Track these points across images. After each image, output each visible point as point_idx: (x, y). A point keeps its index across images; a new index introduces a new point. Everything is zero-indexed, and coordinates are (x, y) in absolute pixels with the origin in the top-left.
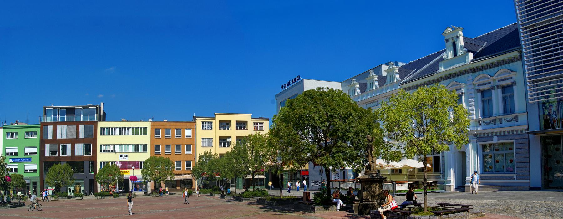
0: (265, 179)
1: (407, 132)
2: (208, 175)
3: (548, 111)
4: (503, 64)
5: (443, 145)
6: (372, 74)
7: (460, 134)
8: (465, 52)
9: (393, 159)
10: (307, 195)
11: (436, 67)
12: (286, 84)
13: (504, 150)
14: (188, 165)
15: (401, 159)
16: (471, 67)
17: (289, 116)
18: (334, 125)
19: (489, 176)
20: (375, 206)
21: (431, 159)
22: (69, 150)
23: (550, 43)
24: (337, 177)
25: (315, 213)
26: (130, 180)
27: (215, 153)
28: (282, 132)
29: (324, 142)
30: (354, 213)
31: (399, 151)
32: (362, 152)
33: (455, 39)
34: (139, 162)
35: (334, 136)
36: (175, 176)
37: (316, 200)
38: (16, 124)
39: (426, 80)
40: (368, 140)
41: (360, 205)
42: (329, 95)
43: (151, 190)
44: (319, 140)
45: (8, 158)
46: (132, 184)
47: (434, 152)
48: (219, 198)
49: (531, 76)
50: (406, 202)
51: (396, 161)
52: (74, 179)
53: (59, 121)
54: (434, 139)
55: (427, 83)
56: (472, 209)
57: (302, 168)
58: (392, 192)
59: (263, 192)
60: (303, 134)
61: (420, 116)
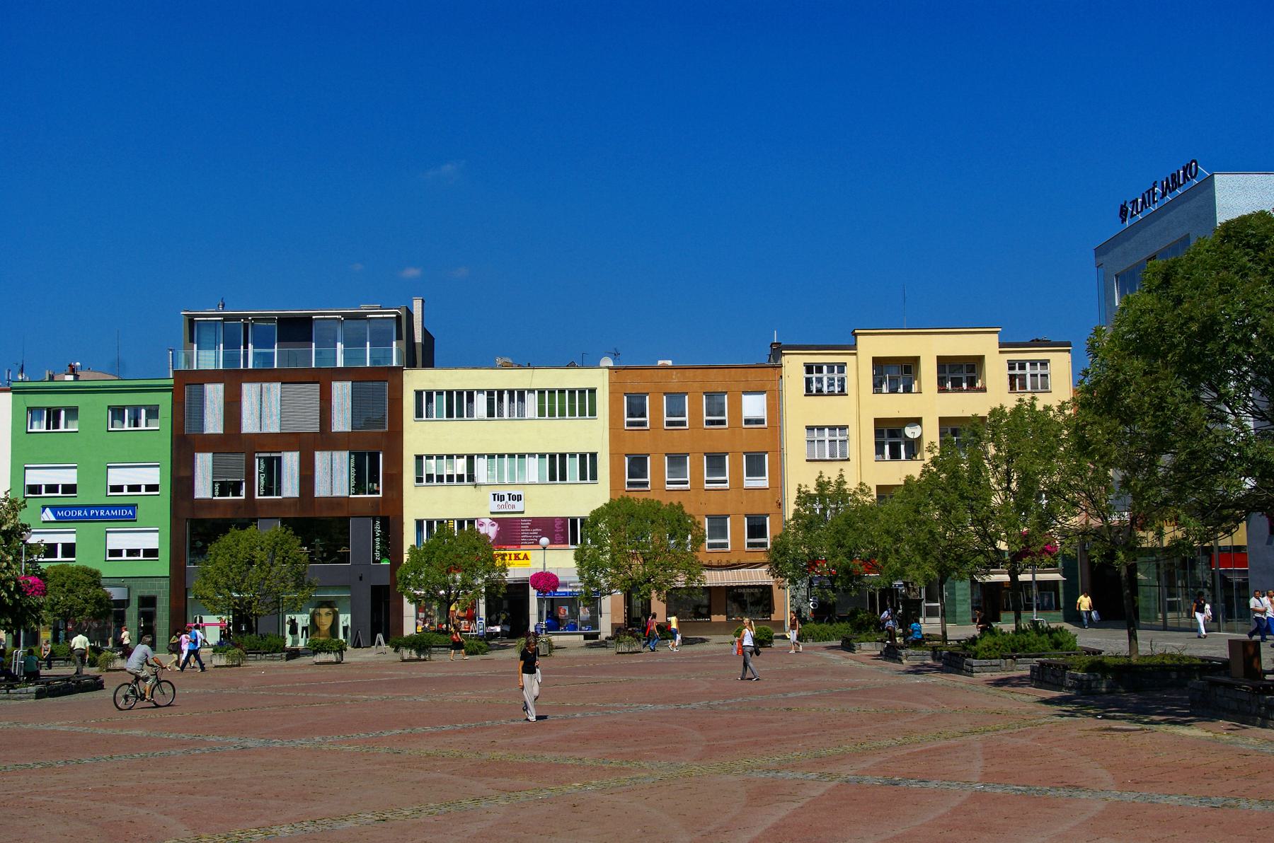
0: (1061, 585)
2: (834, 567)
12: (1140, 200)
14: (757, 529)
17: (1160, 329)
22: (292, 477)
26: (531, 588)
27: (861, 484)
28: (1132, 394)
34: (564, 519)
36: (706, 573)
38: (71, 378)
43: (612, 624)
45: (34, 503)
46: (540, 602)
48: (876, 658)
52: (310, 585)
53: (250, 366)
59: (1056, 635)
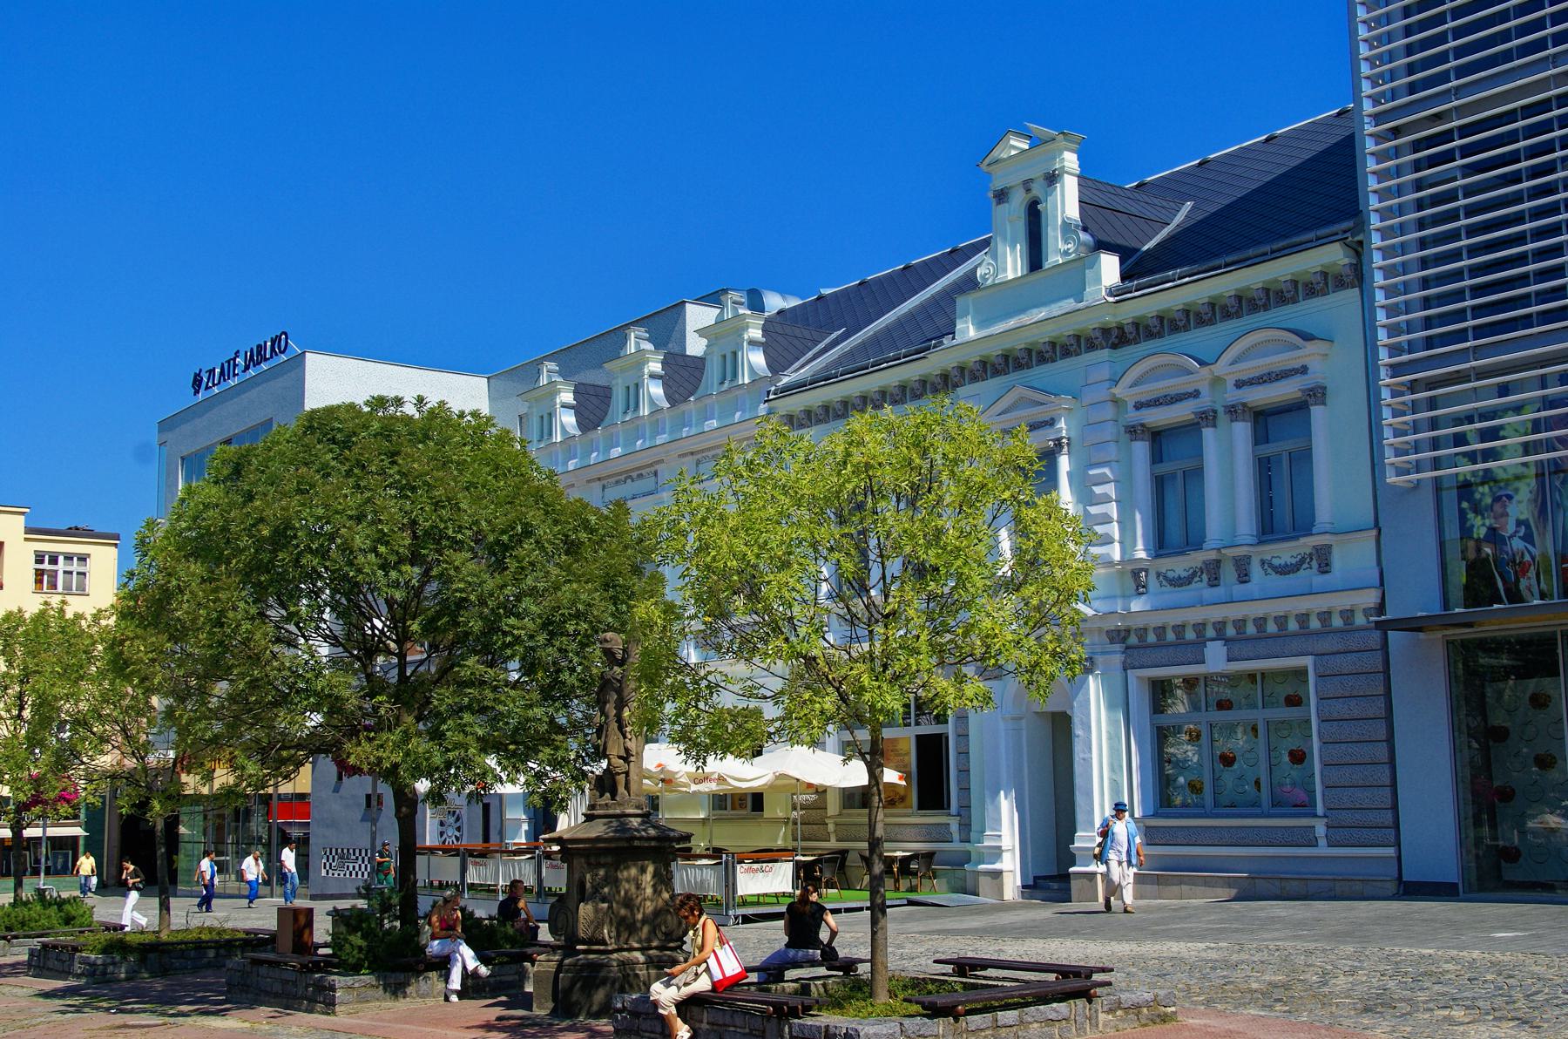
0: (81, 842)
1: (791, 619)
3: (1487, 522)
4: (1266, 308)
5: (961, 679)
6: (636, 341)
7: (1043, 630)
8: (1082, 249)
9: (725, 746)
10: (296, 919)
11: (941, 321)
13: (1260, 705)
15: (761, 747)
16: (1110, 319)
17: (225, 529)
18: (445, 580)
19: (1215, 828)
20: (637, 976)
21: (902, 746)
23: (1517, 198)
24: (451, 832)
25: (334, 1013)
28: (185, 606)
29: (395, 660)
30: (530, 1009)
31: (752, 706)
32: (578, 709)
33: (1037, 190)
35: (445, 631)
37: (341, 948)
39: (870, 383)
40: (608, 653)
41: (560, 964)
42: (427, 437)
44: (370, 649)
47: (917, 715)
49: (1405, 358)
50: (785, 952)
51: (739, 755)
54: (919, 653)
55: (892, 395)
56: (1109, 984)
57: (276, 785)
58: (718, 904)
59: (67, 907)
60: (288, 619)
61: (857, 547)
